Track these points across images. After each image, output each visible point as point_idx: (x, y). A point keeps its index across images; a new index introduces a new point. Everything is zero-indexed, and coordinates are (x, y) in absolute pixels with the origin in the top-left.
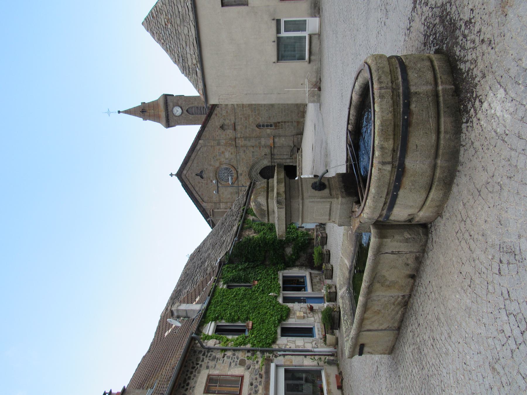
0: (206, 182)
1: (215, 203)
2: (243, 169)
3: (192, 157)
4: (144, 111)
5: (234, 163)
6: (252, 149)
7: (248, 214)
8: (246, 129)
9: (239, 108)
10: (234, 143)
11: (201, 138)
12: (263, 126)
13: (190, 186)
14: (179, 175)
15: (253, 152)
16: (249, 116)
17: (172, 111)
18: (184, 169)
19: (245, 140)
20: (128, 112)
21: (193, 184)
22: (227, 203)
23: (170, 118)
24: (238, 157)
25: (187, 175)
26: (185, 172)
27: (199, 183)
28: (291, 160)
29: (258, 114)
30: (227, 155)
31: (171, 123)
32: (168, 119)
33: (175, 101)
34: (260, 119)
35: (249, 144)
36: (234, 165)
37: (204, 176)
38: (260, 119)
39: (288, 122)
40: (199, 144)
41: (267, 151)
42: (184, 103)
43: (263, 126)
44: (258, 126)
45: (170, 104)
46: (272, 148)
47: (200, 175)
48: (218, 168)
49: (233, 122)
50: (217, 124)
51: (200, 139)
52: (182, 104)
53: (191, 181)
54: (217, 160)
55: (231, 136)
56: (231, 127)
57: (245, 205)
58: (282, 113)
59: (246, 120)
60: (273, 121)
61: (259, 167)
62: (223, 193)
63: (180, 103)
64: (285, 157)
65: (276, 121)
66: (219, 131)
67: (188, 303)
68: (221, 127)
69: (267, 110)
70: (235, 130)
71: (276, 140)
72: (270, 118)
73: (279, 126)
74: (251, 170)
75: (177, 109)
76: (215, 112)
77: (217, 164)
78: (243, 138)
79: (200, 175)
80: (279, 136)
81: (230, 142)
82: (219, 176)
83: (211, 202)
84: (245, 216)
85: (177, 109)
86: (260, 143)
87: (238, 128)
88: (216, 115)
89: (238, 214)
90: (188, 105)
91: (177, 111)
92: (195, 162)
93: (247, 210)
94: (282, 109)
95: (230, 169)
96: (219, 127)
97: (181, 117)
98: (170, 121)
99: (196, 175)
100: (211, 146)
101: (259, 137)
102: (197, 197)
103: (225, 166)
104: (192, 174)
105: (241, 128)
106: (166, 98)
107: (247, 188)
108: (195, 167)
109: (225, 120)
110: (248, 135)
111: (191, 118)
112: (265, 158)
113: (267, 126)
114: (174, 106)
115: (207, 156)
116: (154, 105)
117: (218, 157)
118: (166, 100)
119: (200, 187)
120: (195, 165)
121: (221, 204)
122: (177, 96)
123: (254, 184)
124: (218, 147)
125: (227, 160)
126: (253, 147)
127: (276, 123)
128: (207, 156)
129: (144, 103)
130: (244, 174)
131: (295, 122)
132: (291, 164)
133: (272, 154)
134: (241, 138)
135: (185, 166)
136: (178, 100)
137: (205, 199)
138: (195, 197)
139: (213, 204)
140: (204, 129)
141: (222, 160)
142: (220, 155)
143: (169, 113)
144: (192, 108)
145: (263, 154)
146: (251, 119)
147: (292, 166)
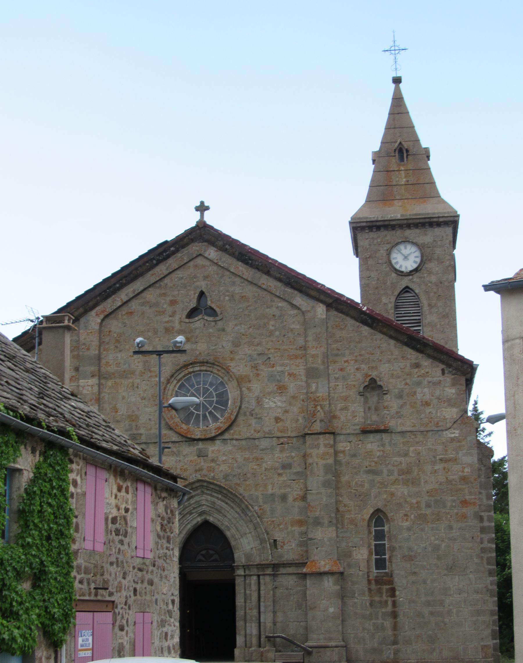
0: (177, 326)
1: (99, 358)
2: (223, 460)
3: (265, 281)
4: (401, 155)
5: (242, 430)
6: (296, 491)
7: (43, 454)
8: (369, 472)
9: (440, 448)
10: (317, 427)
11: (334, 313)
12: (380, 536)
13: (162, 269)
14: (202, 234)
15: (284, 498)
16: (415, 482)
17: (406, 241)
18: (223, 249)
19: (327, 469)
20: (398, 107)
21: (167, 281)
22: (99, 400)
23: (383, 233)
24: (264, 443)
25: (200, 261)
26: (212, 253)
27: (173, 303)
28: (254, 641)
29: (422, 518)
30: (274, 404)
31: (365, 239)
32: (378, 228)
33: (438, 251)
34: (406, 524)
35: (315, 482)
36: (235, 428)
37: (198, 322)
38: (406, 524)
39: (395, 627)
40: (312, 302)
41: (290, 551)
42: (433, 278)
43: (380, 536)
44: (379, 517)
45: (428, 236)
46: (301, 569)
47: (201, 308)
48: (227, 371)
49: (392, 424)
50: (384, 368)
51: (329, 306)
52: (430, 273)
53: (179, 273)
54: (255, 367)
55: (342, 417)
56: (375, 418)
57: (82, 440)
58: (428, 604)
59: (401, 472)
60: (398, 569)
61: (228, 520)
62: (134, 387)
63: (429, 265)
64: (267, 618)
65: (399, 581)
66: (359, 376)
67: (134, 655)
68: (373, 381)
69: (436, 548)
70: (365, 432)
71: (329, 584)
72: (410, 558)
73: (380, 591)
74: (220, 490)
75: (412, 258)
76: (426, 362)
77: (239, 368)
78: (336, 461)
79: (201, 308)
80: (343, 596)
81: (320, 415)
82: (197, 374)
83: (101, 343)
84: (32, 435)
85: (412, 258)
86: (317, 522)
87: (372, 444)
88: (417, 366)
89: (49, 415)
90: (427, 292)
91: (406, 258)
92: (249, 291)
93: (63, 449)
94: (442, 603)
95: (222, 412)
96: (374, 374)
97: (385, 268)
98: (372, 235)
99: (202, 294)
100: (304, 348)
101: (338, 518)
102: (123, 295)
103: (232, 394)
104: (206, 277)
105: (369, 454)
106: (446, 223)
107: (154, 461)
108: (229, 289)
109: (400, 396)
110: (344, 479)
111: (384, 300)
112: (262, 542)
113: (380, 550)
114: (421, 247)
115: (271, 334)
116: (423, 184)
117: (265, 371)
118: (439, 224)
119: (156, 304)
120: (237, 290)
121: (94, 381)
122: (453, 258)
123: (172, 492)
124: (301, 371)
125: (254, 403)
126: (304, 498)
127: (391, 582)
128: (271, 334)
129: (428, 157)
130: (203, 463)
131: (396, 652)
132: (240, 640)
133: (276, 567)
134: (336, 453)
135: (232, 255)
136: (440, 261)
137: (114, 326)
138: (122, 286)
139: (93, 351)
140: (364, 323)
141: (256, 387)
142: (271, 377)
143: (399, 233)
144: (417, 305)
145: (278, 536)
146: (402, 491)
147: (234, 645)
